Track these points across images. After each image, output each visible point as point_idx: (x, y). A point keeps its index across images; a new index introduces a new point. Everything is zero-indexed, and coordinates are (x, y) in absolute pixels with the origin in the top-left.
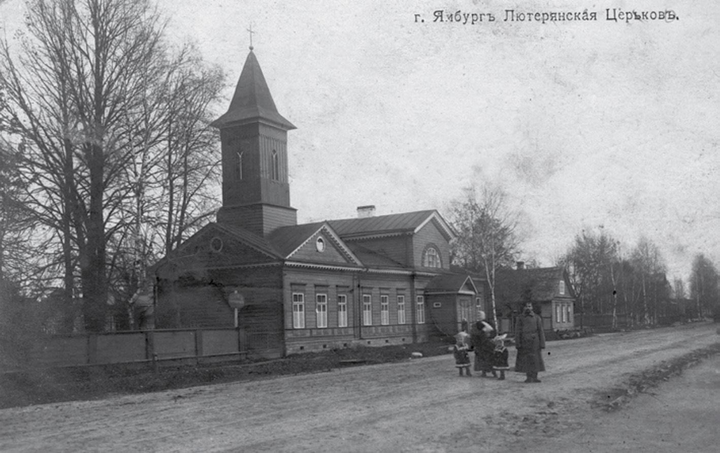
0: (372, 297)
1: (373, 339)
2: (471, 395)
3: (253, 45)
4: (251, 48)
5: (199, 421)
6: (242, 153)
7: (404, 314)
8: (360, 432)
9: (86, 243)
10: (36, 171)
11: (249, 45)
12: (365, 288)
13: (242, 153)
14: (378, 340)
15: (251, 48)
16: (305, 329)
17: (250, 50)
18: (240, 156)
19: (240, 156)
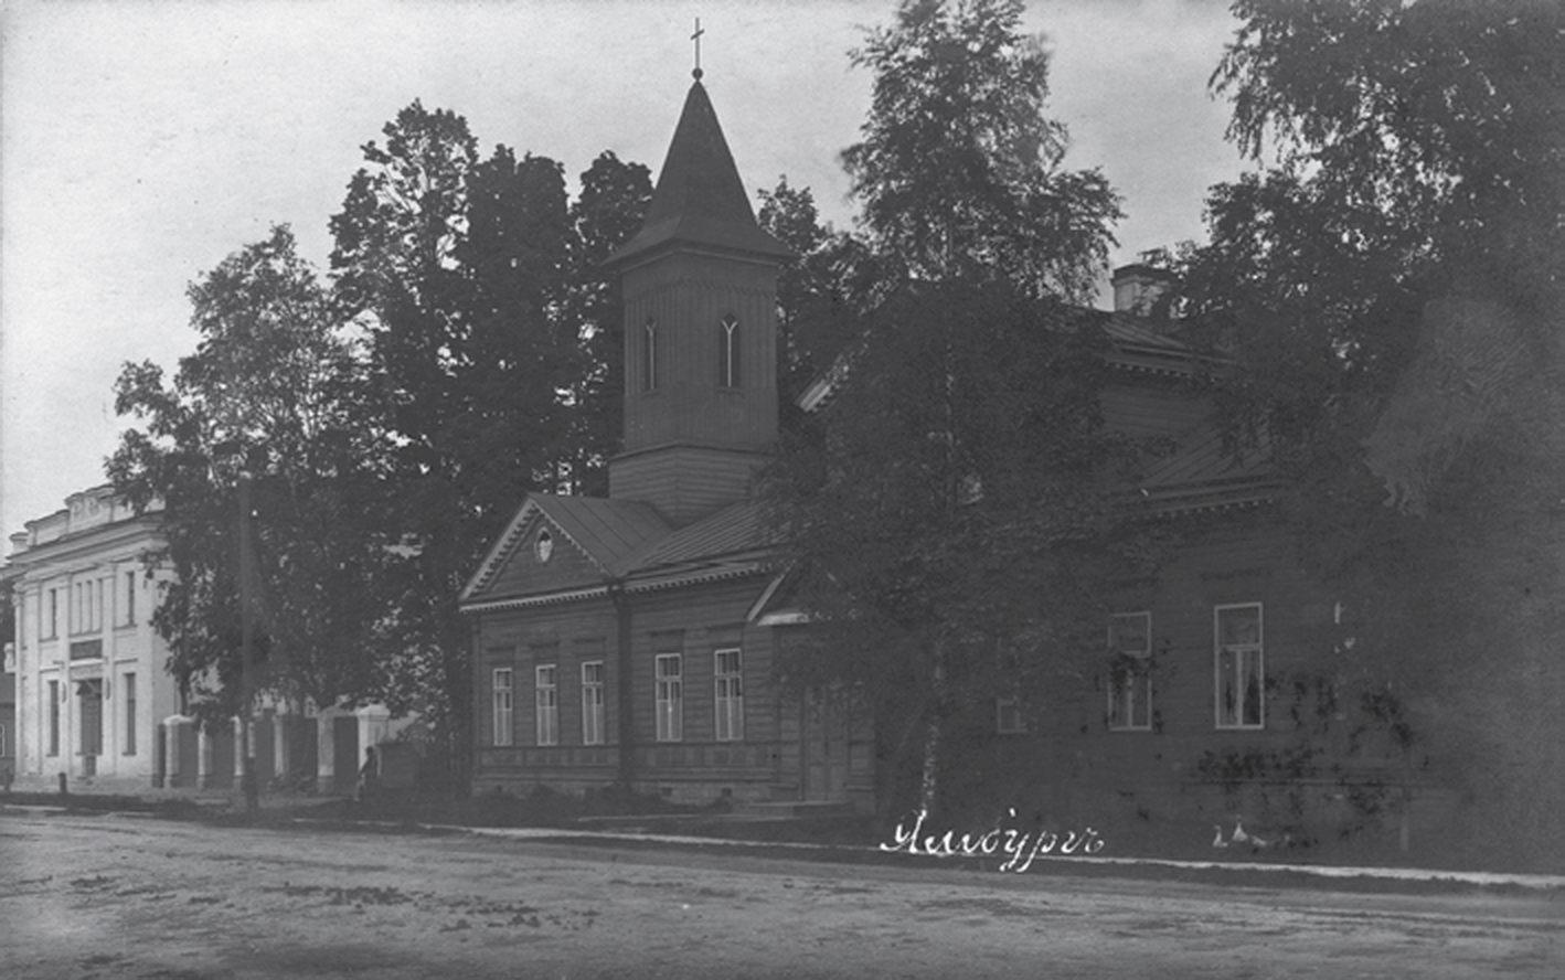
0: (743, 652)
1: (683, 781)
2: (1026, 914)
3: (701, 67)
4: (698, 73)
5: (727, 936)
6: (733, 326)
7: (555, 716)
8: (1043, 940)
9: (1353, 639)
10: (349, 325)
11: (694, 67)
12: (101, 589)
13: (733, 326)
14: (697, 785)
15: (698, 73)
16: (559, 748)
17: (694, 80)
18: (730, 332)
19: (730, 332)
